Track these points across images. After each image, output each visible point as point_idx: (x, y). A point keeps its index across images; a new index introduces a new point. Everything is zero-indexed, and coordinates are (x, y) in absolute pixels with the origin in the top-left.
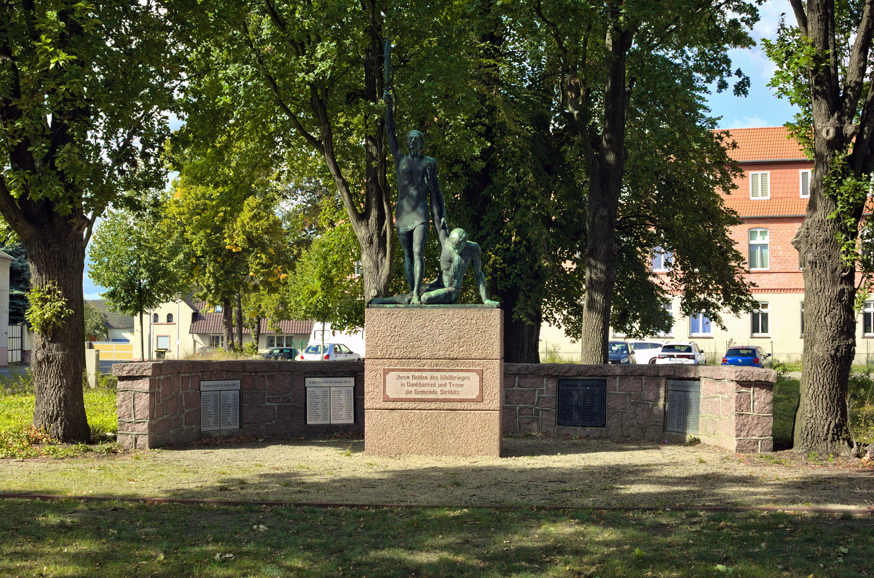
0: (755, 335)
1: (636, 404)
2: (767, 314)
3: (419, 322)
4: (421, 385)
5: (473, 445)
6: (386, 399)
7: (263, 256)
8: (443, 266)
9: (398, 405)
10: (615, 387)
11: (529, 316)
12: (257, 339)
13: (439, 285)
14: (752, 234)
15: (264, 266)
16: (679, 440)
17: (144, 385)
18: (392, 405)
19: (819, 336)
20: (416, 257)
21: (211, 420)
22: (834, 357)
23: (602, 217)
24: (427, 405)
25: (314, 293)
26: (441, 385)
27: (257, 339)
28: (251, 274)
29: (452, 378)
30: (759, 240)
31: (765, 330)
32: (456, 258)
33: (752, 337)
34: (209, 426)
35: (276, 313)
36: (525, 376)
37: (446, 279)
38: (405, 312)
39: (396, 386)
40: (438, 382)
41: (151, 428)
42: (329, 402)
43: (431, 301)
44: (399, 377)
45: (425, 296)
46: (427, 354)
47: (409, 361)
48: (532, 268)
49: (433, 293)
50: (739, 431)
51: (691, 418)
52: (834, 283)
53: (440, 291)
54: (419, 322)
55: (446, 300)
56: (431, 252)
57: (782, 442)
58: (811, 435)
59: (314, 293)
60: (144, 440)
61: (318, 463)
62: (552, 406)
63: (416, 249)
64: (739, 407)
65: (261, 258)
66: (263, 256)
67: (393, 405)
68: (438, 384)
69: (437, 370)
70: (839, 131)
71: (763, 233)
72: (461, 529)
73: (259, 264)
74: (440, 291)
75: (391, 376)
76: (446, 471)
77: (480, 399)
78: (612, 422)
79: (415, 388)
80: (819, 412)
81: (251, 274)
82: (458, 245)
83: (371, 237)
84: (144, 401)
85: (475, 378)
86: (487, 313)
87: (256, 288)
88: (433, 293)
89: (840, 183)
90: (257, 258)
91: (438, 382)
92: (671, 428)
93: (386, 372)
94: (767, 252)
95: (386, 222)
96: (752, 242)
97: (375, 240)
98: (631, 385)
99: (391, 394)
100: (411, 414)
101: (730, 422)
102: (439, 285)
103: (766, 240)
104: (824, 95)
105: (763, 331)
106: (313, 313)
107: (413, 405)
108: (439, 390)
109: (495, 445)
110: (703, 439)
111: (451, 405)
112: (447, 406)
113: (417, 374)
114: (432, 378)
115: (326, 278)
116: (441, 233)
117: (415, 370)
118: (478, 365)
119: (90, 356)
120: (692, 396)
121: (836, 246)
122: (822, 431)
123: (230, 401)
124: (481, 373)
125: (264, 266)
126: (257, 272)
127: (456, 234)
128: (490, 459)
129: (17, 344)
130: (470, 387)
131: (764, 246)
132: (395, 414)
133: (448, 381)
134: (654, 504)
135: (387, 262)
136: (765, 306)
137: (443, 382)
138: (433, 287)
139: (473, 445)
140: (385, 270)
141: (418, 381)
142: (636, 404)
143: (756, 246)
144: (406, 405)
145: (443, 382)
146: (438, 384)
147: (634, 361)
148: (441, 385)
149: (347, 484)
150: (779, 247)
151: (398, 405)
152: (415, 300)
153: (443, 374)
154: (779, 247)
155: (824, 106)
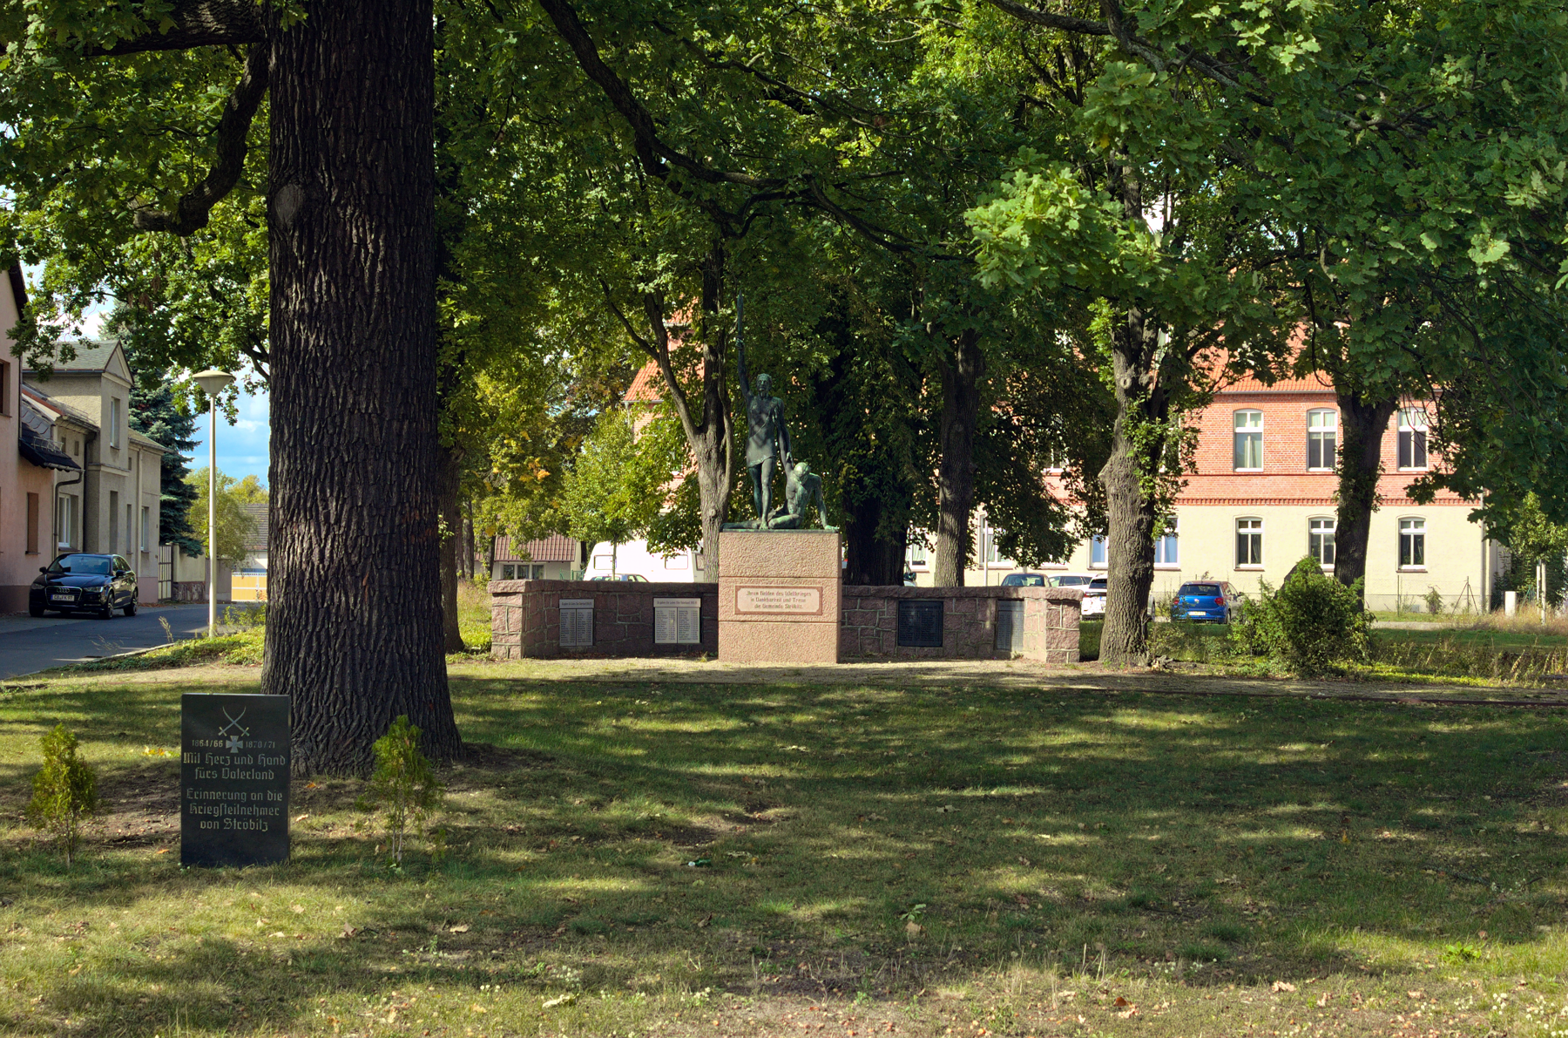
0: (1242, 566)
1: (971, 624)
2: (1259, 536)
3: (767, 545)
5: (816, 649)
6: (738, 612)
7: (513, 443)
8: (788, 495)
9: (748, 617)
10: (951, 608)
11: (894, 534)
12: (490, 569)
13: (785, 512)
14: (1239, 418)
15: (513, 458)
16: (1005, 656)
17: (517, 601)
18: (743, 618)
19: (1119, 560)
20: (764, 487)
21: (568, 636)
22: (1132, 579)
23: (958, 434)
24: (773, 618)
25: (622, 504)
27: (490, 569)
28: (495, 470)
30: (1249, 427)
31: (1256, 559)
32: (800, 488)
33: (1237, 570)
34: (567, 642)
35: (523, 528)
36: (867, 597)
37: (790, 507)
38: (755, 536)
39: (746, 600)
41: (523, 639)
42: (675, 621)
43: (777, 526)
45: (772, 522)
46: (773, 573)
47: (758, 579)
48: (895, 478)
49: (779, 520)
50: (1049, 643)
51: (1014, 639)
52: (1134, 513)
53: (786, 518)
54: (767, 545)
55: (791, 526)
56: (778, 480)
57: (1088, 656)
58: (1114, 649)
59: (622, 504)
60: (516, 651)
62: (892, 628)
63: (764, 480)
64: (1050, 623)
65: (509, 447)
66: (513, 443)
67: (744, 617)
68: (784, 599)
70: (1135, 381)
71: (1255, 417)
73: (506, 455)
74: (786, 518)
75: (742, 592)
76: (790, 670)
77: (820, 613)
78: (948, 642)
80: (1120, 628)
81: (495, 470)
82: (801, 478)
83: (709, 453)
84: (517, 615)
85: (816, 594)
86: (827, 537)
87: (497, 492)
88: (779, 520)
89: (1135, 427)
90: (503, 446)
92: (999, 642)
93: (738, 589)
94: (1261, 445)
95: (727, 436)
96: (1238, 430)
97: (714, 455)
98: (965, 606)
99: (742, 608)
100: (759, 625)
101: (1042, 635)
102: (785, 512)
103: (1260, 427)
104: (1121, 349)
105: (1254, 561)
106: (601, 530)
107: (761, 618)
109: (833, 652)
110: (1026, 654)
111: (795, 618)
112: (791, 618)
115: (636, 485)
116: (787, 466)
118: (819, 583)
120: (1016, 615)
121: (1136, 481)
122: (1122, 644)
123: (585, 619)
124: (821, 590)
125: (513, 458)
126: (503, 467)
127: (800, 468)
128: (832, 664)
129: (165, 573)
130: (811, 602)
131: (1255, 437)
132: (746, 625)
134: (943, 684)
135: (726, 480)
136: (1256, 524)
138: (779, 514)
139: (816, 649)
140: (724, 488)
142: (971, 624)
143: (1244, 435)
144: (755, 618)
146: (784, 599)
149: (710, 673)
150: (1278, 437)
151: (748, 617)
152: (763, 526)
154: (1278, 437)
155: (1122, 359)
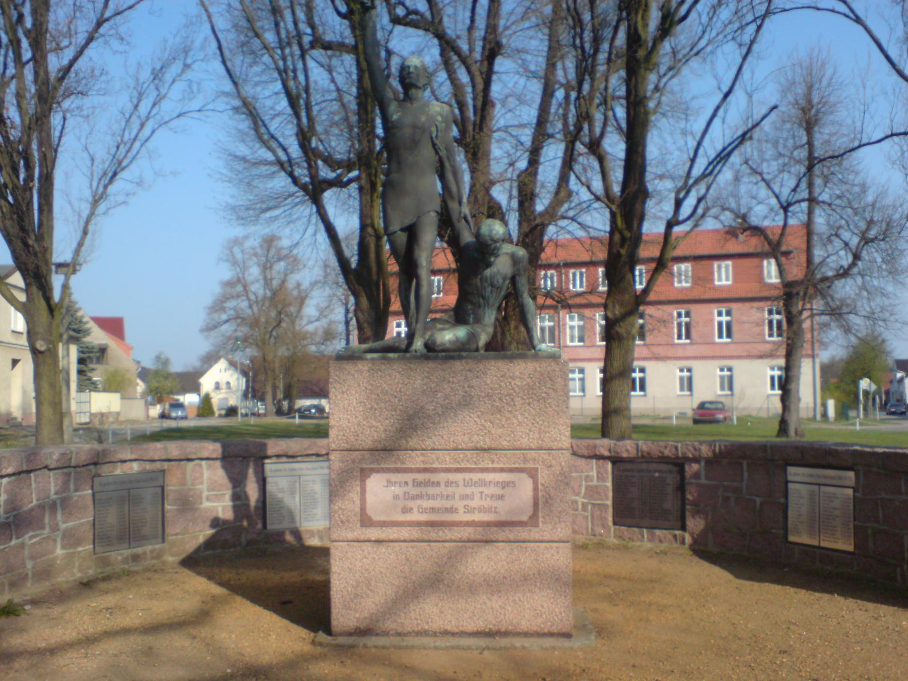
4: (429, 497)
18: (374, 533)
26: (464, 497)
29: (483, 483)
40: (461, 490)
44: (390, 483)
61: (73, 386)
69: (458, 470)
72: (488, 26)
79: (419, 502)
91: (461, 490)
108: (459, 505)
113: (420, 477)
114: (448, 483)
117: (419, 471)
119: (801, 537)
133: (476, 490)
137: (468, 491)
141: (424, 490)
145: (468, 491)
147: (802, 360)
148: (464, 497)
153: (468, 476)
